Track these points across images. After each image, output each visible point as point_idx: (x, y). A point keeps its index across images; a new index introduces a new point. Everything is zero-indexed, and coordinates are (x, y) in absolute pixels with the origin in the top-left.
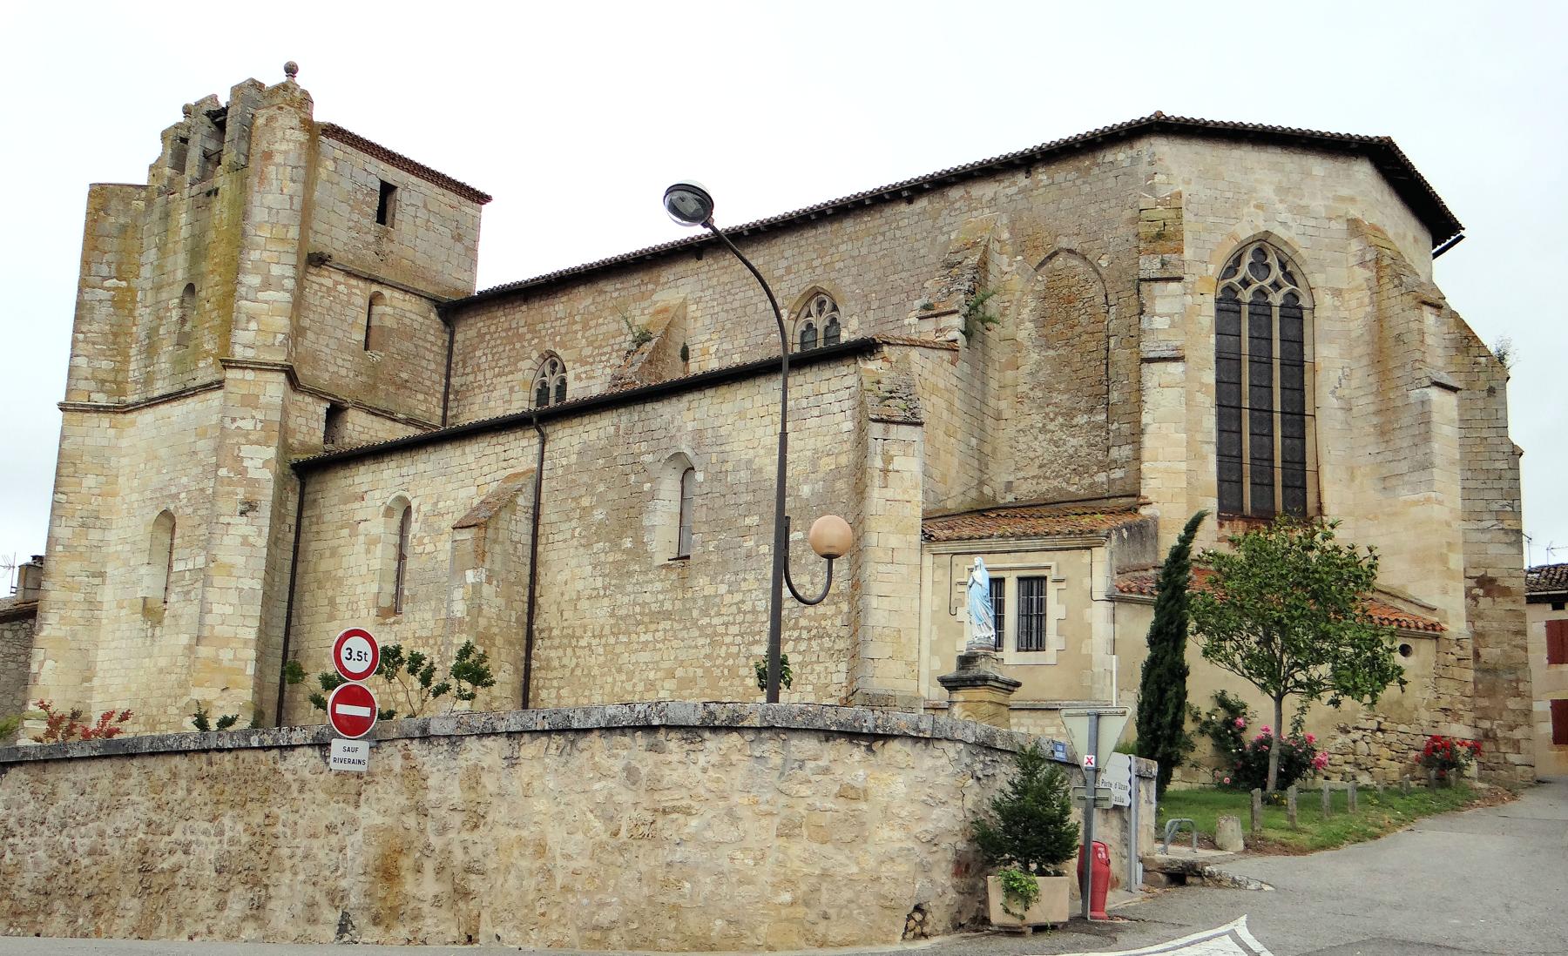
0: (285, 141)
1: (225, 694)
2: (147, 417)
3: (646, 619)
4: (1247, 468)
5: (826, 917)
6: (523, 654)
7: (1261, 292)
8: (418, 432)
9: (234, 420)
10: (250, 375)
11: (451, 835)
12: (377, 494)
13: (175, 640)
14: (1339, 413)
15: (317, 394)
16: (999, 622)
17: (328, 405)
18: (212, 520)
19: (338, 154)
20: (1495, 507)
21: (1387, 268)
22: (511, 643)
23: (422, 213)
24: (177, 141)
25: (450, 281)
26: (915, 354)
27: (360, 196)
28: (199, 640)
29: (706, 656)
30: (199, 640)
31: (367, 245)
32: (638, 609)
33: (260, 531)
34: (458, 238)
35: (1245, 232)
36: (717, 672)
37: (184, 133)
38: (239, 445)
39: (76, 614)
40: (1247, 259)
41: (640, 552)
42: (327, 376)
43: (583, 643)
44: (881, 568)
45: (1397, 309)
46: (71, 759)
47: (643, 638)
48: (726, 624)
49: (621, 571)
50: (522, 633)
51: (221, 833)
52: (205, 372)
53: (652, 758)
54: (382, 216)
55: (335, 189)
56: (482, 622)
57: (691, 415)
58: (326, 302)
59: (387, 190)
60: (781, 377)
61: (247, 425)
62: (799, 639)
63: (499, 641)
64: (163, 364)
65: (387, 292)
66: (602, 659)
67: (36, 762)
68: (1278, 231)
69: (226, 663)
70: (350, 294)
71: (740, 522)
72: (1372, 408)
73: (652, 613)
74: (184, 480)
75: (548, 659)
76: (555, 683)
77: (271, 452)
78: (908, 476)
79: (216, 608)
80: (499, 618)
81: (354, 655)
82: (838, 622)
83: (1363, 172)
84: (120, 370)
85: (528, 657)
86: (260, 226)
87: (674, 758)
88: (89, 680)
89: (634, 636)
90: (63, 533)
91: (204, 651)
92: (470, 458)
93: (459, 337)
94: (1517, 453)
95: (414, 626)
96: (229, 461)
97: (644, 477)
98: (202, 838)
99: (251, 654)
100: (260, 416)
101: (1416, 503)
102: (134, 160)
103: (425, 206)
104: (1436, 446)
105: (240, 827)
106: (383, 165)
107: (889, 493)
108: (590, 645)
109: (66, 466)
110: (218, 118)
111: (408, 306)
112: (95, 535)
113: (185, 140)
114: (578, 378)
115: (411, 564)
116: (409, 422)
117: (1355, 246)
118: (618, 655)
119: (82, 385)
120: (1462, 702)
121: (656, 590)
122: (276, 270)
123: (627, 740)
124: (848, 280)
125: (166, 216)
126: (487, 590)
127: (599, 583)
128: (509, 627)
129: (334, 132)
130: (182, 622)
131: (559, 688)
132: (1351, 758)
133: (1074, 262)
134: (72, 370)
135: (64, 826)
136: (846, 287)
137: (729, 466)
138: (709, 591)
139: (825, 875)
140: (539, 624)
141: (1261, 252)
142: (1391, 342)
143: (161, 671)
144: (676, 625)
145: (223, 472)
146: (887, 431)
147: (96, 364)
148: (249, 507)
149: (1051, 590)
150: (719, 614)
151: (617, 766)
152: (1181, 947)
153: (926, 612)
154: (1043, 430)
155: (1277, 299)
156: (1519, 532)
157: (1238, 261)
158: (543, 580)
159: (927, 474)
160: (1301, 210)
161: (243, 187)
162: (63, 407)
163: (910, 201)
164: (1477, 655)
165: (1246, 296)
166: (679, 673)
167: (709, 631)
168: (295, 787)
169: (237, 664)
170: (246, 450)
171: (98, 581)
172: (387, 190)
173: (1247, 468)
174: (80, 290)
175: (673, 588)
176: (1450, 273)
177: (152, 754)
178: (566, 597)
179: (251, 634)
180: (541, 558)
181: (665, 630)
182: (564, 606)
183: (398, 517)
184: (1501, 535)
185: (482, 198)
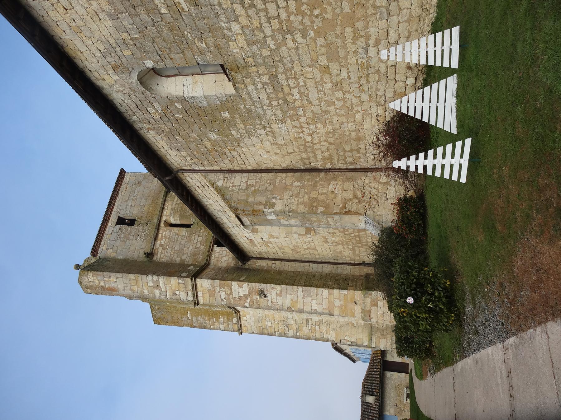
1: (357, 302)
3: (281, 95)
6: (322, 174)
9: (222, 300)
10: (200, 294)
17: (215, 246)
19: (105, 248)
22: (315, 185)
23: (130, 203)
27: (122, 236)
29: (304, 36)
31: (144, 230)
32: (274, 103)
33: (273, 288)
34: (140, 183)
36: (318, 23)
38: (233, 298)
39: (325, 329)
41: (227, 103)
42: (202, 247)
43: (309, 139)
47: (297, 97)
48: (269, 19)
49: (249, 118)
50: (307, 176)
55: (120, 248)
56: (301, 209)
58: (169, 250)
59: (121, 221)
61: (223, 295)
63: (314, 195)
65: (164, 218)
66: (319, 125)
69: (342, 303)
70: (165, 237)
71: (168, 18)
75: (324, 159)
76: (341, 153)
77: (234, 284)
79: (314, 307)
80: (297, 195)
84: (222, 313)
85: (325, 170)
88: (353, 324)
89: (297, 104)
90: (291, 333)
96: (242, 302)
99: (336, 291)
100: (218, 289)
103: (126, 201)
106: (109, 224)
108: (310, 134)
111: (170, 207)
112: (291, 322)
118: (314, 114)
119: (231, 326)
121: (257, 91)
122: (151, 284)
127: (262, 132)
128: (304, 187)
131: (345, 151)
137: (125, 36)
138: (242, 42)
140: (300, 166)
144: (280, 70)
145: (247, 304)
147: (222, 322)
148: (262, 294)
150: (261, 29)
158: (269, 165)
162: (241, 333)
166: (323, 61)
167: (279, 36)
169: (342, 298)
170: (235, 295)
171: (310, 321)
172: (121, 221)
174: (195, 327)
175: (249, 76)
178: (278, 151)
179: (326, 292)
180: (256, 167)
181: (287, 79)
182: (284, 151)
185: (122, 173)
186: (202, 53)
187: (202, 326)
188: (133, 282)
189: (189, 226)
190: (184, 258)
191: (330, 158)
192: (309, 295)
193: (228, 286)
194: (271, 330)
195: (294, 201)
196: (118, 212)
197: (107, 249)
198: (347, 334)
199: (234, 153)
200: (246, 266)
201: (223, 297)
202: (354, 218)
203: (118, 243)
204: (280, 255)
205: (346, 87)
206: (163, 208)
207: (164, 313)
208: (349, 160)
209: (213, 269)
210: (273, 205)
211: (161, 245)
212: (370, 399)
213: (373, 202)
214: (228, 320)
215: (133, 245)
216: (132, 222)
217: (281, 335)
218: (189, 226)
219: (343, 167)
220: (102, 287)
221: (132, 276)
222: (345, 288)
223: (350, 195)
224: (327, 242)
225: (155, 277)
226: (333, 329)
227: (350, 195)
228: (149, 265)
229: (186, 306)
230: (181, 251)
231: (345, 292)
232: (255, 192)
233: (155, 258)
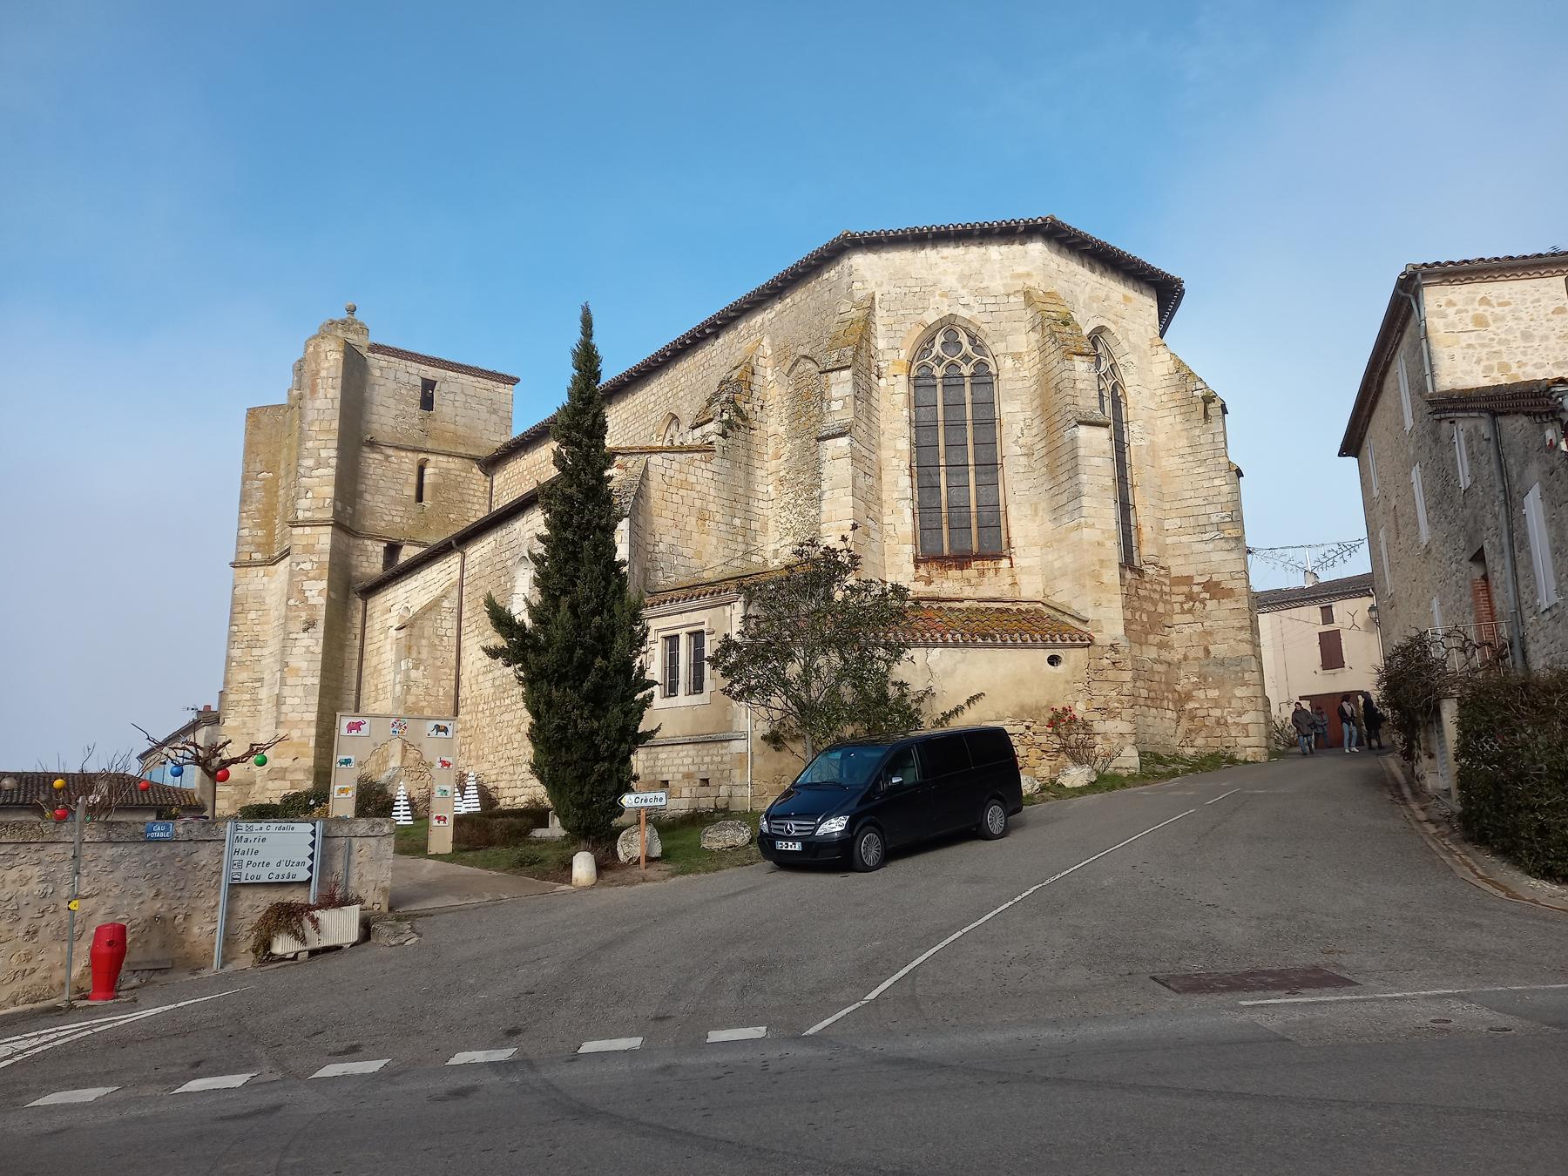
10: (308, 530)
14: (1022, 459)
19: (384, 364)
20: (1214, 519)
23: (461, 397)
34: (495, 412)
35: (931, 317)
40: (940, 339)
50: (451, 704)
59: (428, 385)
61: (307, 566)
65: (432, 458)
68: (963, 313)
72: (1044, 451)
77: (324, 584)
79: (288, 700)
83: (1037, 248)
84: (271, 534)
90: (236, 653)
99: (313, 731)
104: (1084, 478)
111: (452, 466)
112: (256, 652)
117: (1029, 313)
119: (246, 548)
120: (1119, 701)
122: (324, 454)
145: (292, 602)
148: (309, 625)
149: (707, 638)
158: (463, 662)
160: (978, 292)
164: (1207, 651)
172: (428, 385)
174: (243, 483)
179: (313, 717)
184: (1222, 544)
185: (513, 381)
187: (245, 498)
188: (325, 425)
189: (420, 498)
190: (368, 497)
192: (307, 694)
194: (240, 619)
195: (421, 691)
196: (445, 380)
197: (381, 368)
200: (353, 596)
202: (398, 756)
203: (392, 385)
204: (368, 648)
207: (269, 430)
209: (348, 545)
210: (416, 667)
214: (259, 545)
215: (391, 409)
216: (427, 403)
217: (232, 634)
218: (420, 498)
220: (318, 372)
221: (335, 425)
222: (317, 745)
225: (333, 462)
226: (244, 723)
228: (355, 439)
229: (283, 473)
230: (378, 490)
231: (312, 743)
232: (433, 646)
233: (365, 449)
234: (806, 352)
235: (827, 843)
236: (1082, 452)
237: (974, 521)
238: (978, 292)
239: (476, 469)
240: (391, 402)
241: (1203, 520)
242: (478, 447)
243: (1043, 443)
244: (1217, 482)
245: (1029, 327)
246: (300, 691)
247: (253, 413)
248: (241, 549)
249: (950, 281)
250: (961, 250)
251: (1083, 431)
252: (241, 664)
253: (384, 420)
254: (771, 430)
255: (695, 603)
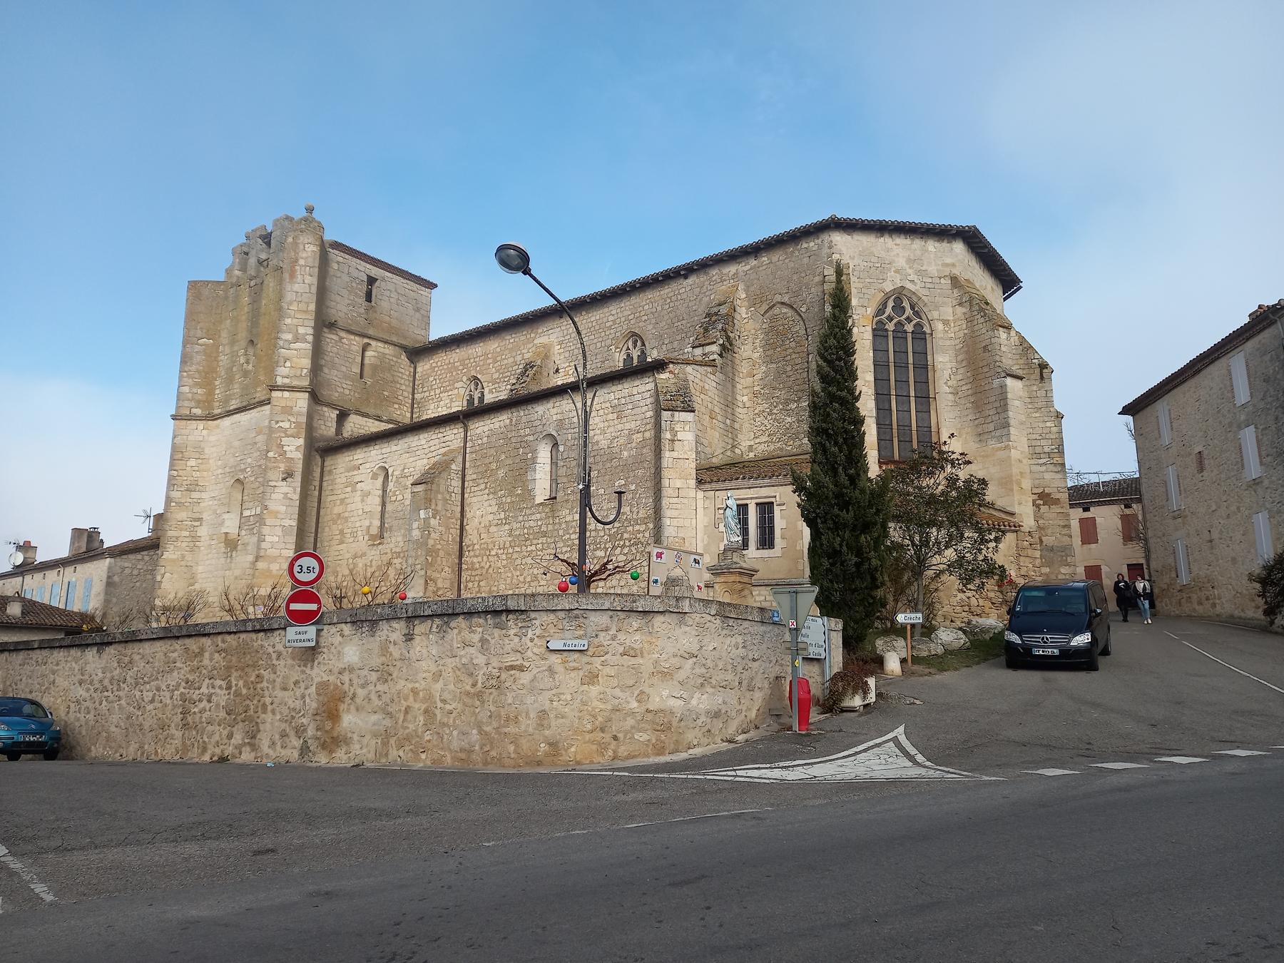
0: (308, 251)
2: (227, 422)
4: (895, 431)
5: (615, 738)
7: (899, 323)
8: (391, 426)
10: (286, 394)
11: (371, 687)
12: (368, 465)
13: (243, 559)
15: (331, 405)
16: (745, 531)
18: (265, 484)
19: (340, 259)
20: (1046, 450)
21: (979, 309)
23: (394, 295)
24: (243, 253)
25: (416, 336)
26: (689, 369)
28: (257, 558)
30: (257, 558)
34: (418, 310)
35: (889, 287)
37: (245, 249)
39: (184, 544)
40: (891, 304)
41: (529, 494)
43: (493, 553)
44: (672, 500)
45: (984, 331)
46: (141, 640)
51: (229, 688)
52: (260, 394)
53: (497, 632)
54: (369, 297)
56: (431, 542)
57: (555, 410)
60: (589, 376)
61: (286, 425)
62: (623, 546)
63: (441, 553)
64: (236, 389)
65: (373, 343)
67: (120, 642)
68: (909, 286)
69: (274, 572)
72: (970, 392)
73: (534, 533)
74: (249, 460)
75: (473, 563)
77: (301, 442)
78: (686, 441)
81: (305, 569)
82: (647, 535)
83: (959, 247)
84: (211, 393)
85: (460, 564)
86: (291, 303)
87: (512, 632)
91: (260, 565)
92: (423, 442)
93: (419, 369)
94: (1059, 416)
95: (392, 545)
97: (527, 450)
98: (218, 691)
101: (1000, 449)
102: (217, 266)
104: (1010, 414)
105: (241, 683)
107: (675, 454)
109: (177, 455)
110: (267, 239)
111: (387, 351)
112: (195, 495)
113: (247, 254)
114: (491, 392)
115: (389, 507)
116: (388, 422)
119: (186, 404)
123: (481, 621)
124: (650, 327)
125: (237, 297)
126: (433, 522)
129: (337, 246)
130: (249, 548)
132: (966, 608)
133: (785, 310)
134: (179, 395)
135: (137, 684)
136: (649, 332)
139: (616, 710)
140: (466, 541)
141: (898, 301)
142: (981, 351)
143: (236, 578)
145: (271, 454)
146: (673, 416)
148: (288, 475)
149: (777, 510)
151: (476, 638)
152: (860, 752)
153: (700, 527)
154: (770, 413)
155: (909, 328)
156: (1063, 465)
157: (885, 305)
158: (468, 515)
159: (698, 442)
160: (921, 273)
161: (281, 282)
162: (174, 418)
163: (686, 277)
164: (1041, 541)
165: (891, 326)
168: (274, 656)
170: (285, 441)
172: (372, 281)
173: (895, 431)
174: (184, 346)
176: (1012, 309)
177: (190, 636)
182: (482, 530)
183: (381, 479)
184: (1051, 467)
185: (432, 286)
186: (564, 489)
187: (185, 359)
190: (326, 370)
191: (473, 569)
193: (298, 433)
196: (383, 279)
197: (338, 263)
198: (175, 576)
199: (483, 486)
201: (281, 424)
205: (535, 583)
206: (386, 342)
208: (470, 585)
211: (342, 338)
212: (15, 610)
213: (677, 591)
214: (199, 401)
217: (171, 478)
219: (463, 579)
220: (296, 261)
223: (440, 585)
224: (355, 557)
225: (310, 338)
226: (183, 557)
227: (440, 585)
232: (445, 500)
234: (786, 299)
235: (1078, 651)
236: (1009, 396)
237: (915, 437)
238: (921, 273)
239: (404, 357)
240: (345, 293)
241: (1038, 450)
242: (405, 338)
243: (969, 386)
244: (1048, 424)
245: (955, 302)
246: (279, 531)
247: (194, 286)
248: (181, 403)
249: (901, 262)
250: (908, 241)
251: (1009, 381)
252: (179, 504)
253: (339, 307)
254: (745, 355)
255: (767, 481)
